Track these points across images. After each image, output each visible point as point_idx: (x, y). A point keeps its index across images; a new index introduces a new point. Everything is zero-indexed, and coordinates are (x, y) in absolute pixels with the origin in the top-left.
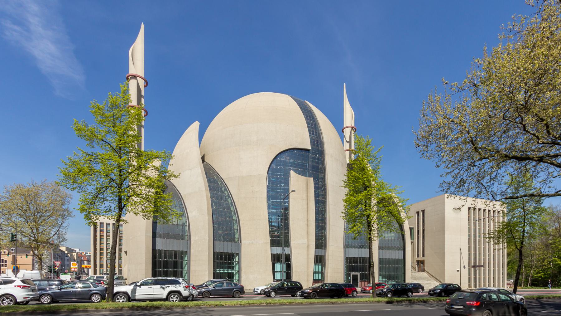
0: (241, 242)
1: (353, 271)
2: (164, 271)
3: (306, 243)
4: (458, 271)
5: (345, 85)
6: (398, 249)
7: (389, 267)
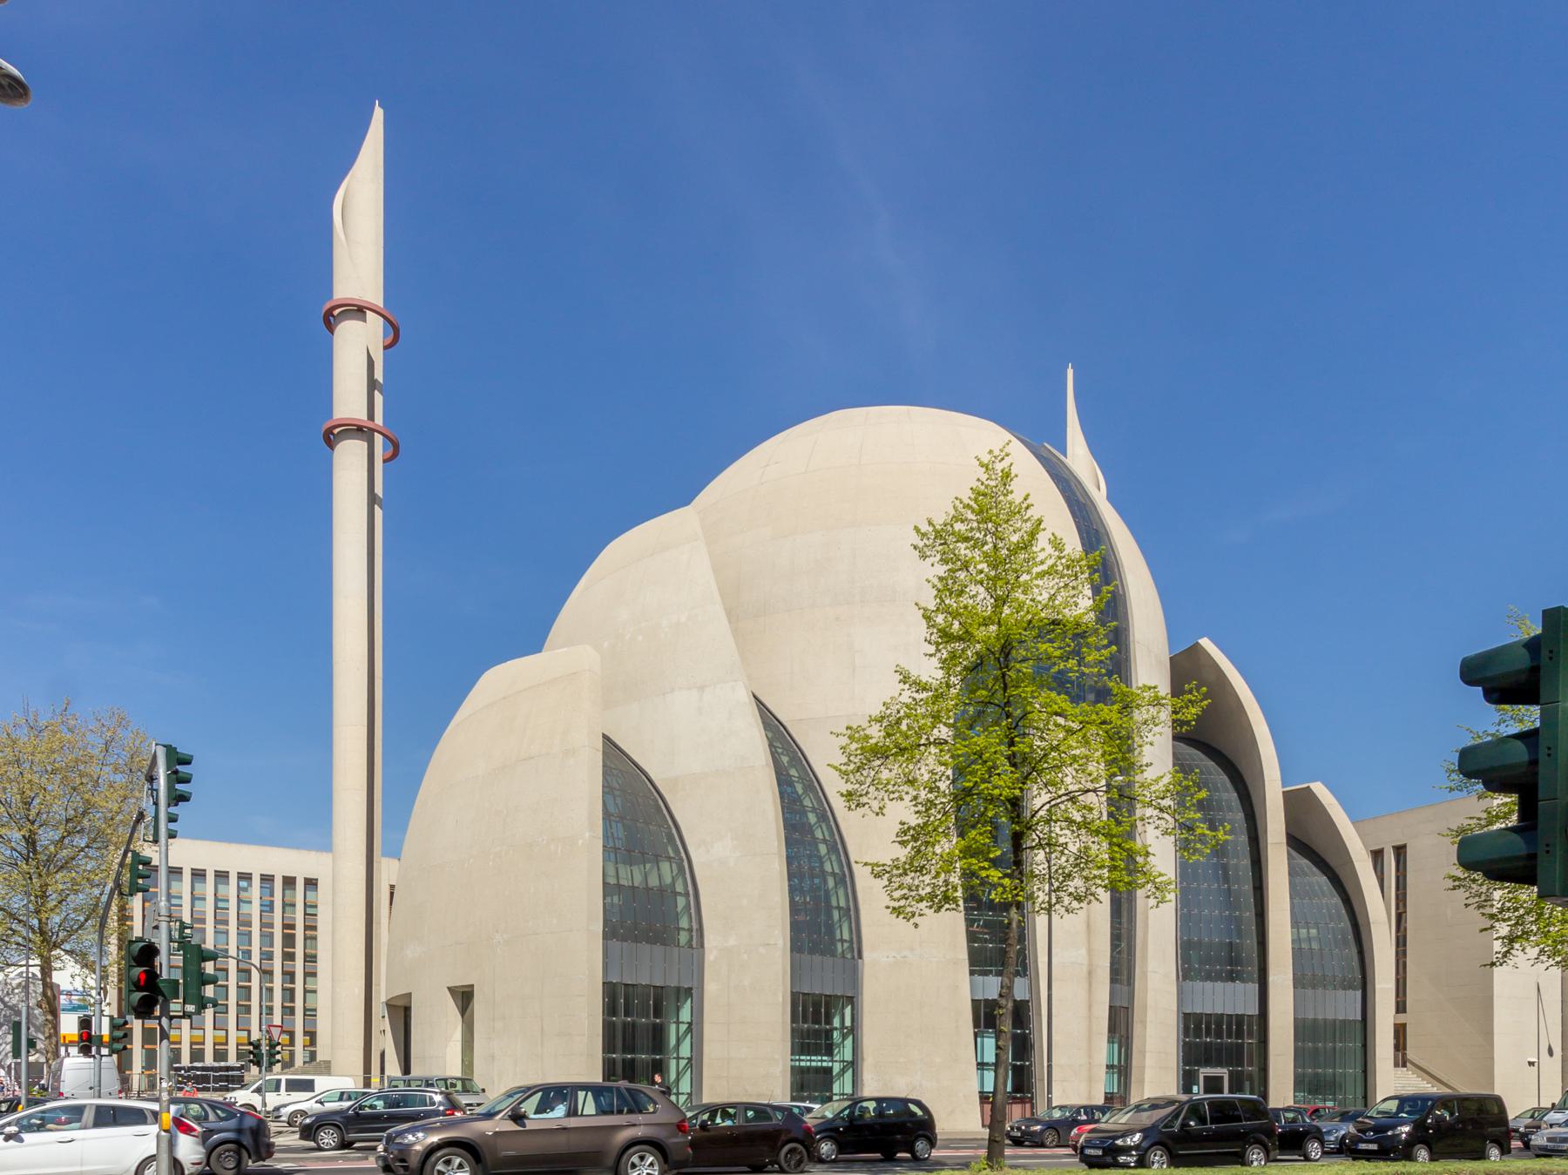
0: (860, 956)
1: (1208, 1063)
2: (624, 1061)
3: (1085, 962)
4: (1531, 1064)
5: (1070, 373)
6: (1347, 986)
7: (1316, 1050)
